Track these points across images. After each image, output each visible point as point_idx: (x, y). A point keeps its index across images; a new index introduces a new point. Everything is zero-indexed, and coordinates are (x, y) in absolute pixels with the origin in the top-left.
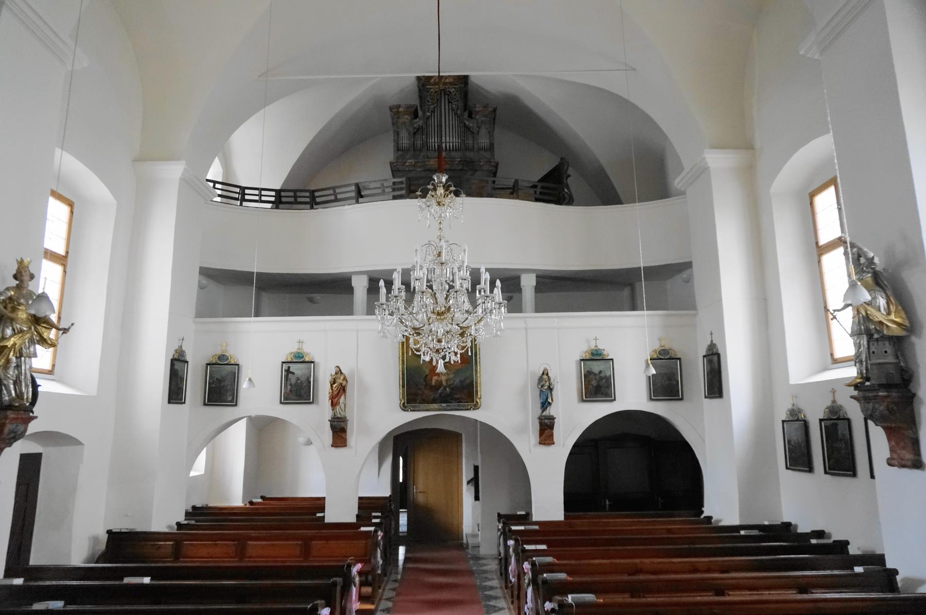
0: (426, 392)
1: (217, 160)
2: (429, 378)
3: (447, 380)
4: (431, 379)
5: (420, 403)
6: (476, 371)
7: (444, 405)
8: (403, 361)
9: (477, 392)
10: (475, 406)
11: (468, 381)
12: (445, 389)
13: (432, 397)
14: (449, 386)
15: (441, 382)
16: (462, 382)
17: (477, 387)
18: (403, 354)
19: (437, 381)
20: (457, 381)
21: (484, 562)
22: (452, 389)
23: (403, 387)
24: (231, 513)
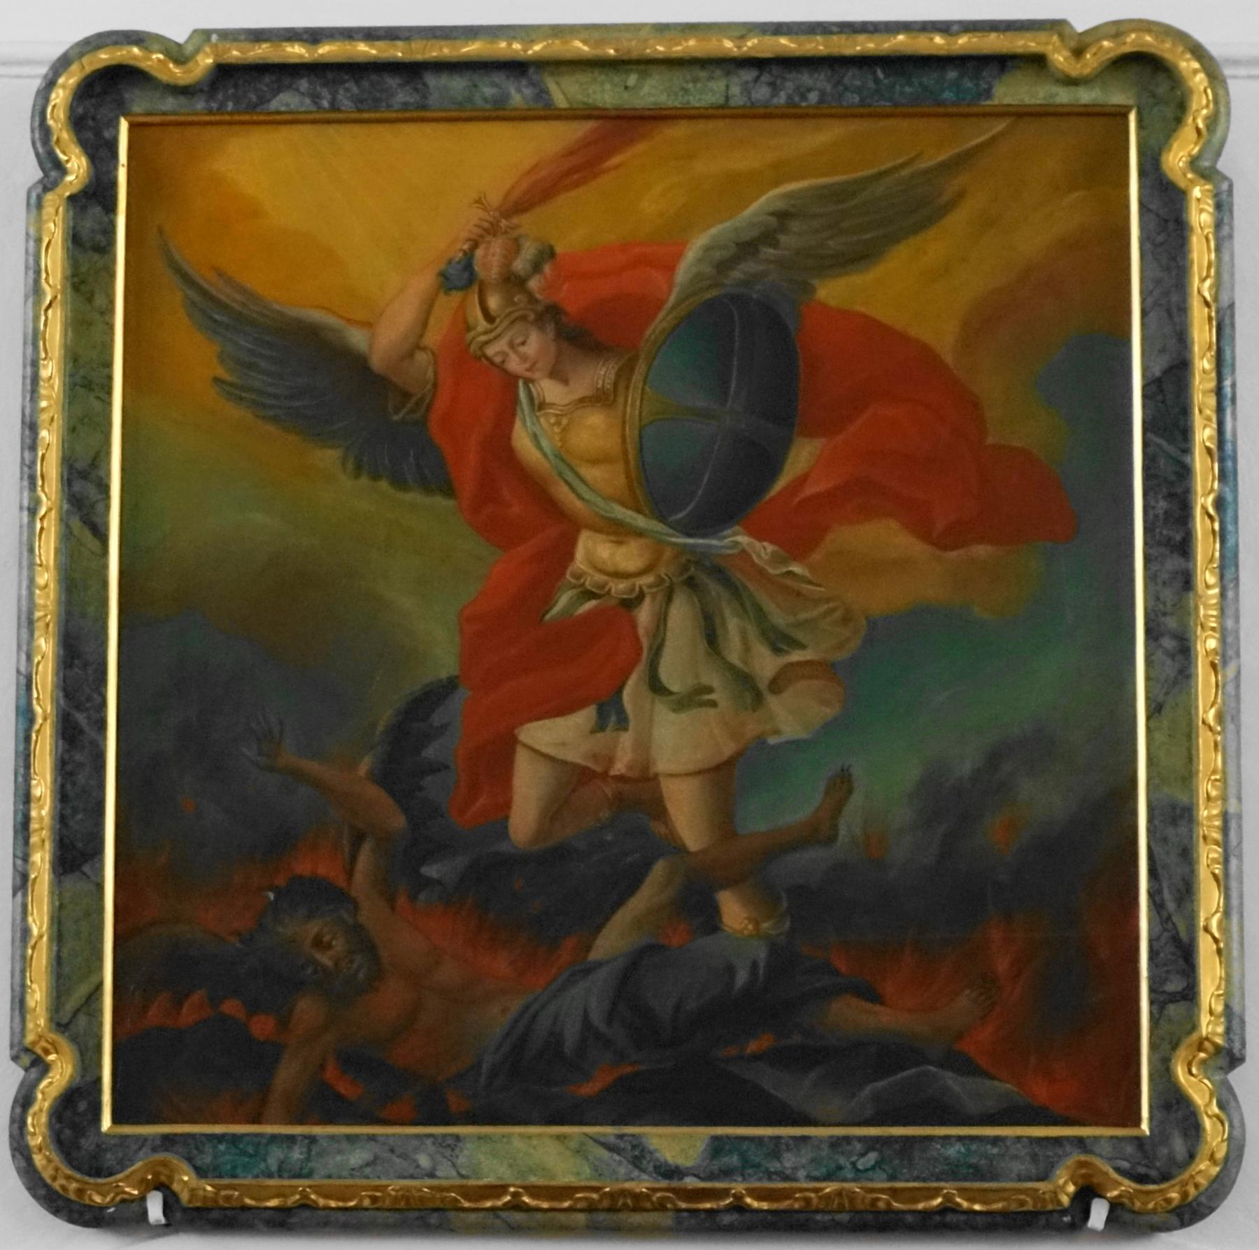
0: (407, 938)
1: (1148, 1133)
2: (451, 744)
3: (725, 779)
4: (497, 757)
5: (326, 1106)
6: (1174, 649)
7: (679, 1144)
8: (82, 478)
9: (1179, 955)
10: (1151, 1165)
11: (1044, 799)
12: (695, 902)
13: (497, 1019)
14: (754, 867)
15: (640, 797)
16: (951, 805)
17: (1178, 891)
18: (86, 381)
19: (574, 779)
20: (886, 786)
21: (544, 1023)
22: (808, 907)
23: (74, 855)
24: (357, 363)
